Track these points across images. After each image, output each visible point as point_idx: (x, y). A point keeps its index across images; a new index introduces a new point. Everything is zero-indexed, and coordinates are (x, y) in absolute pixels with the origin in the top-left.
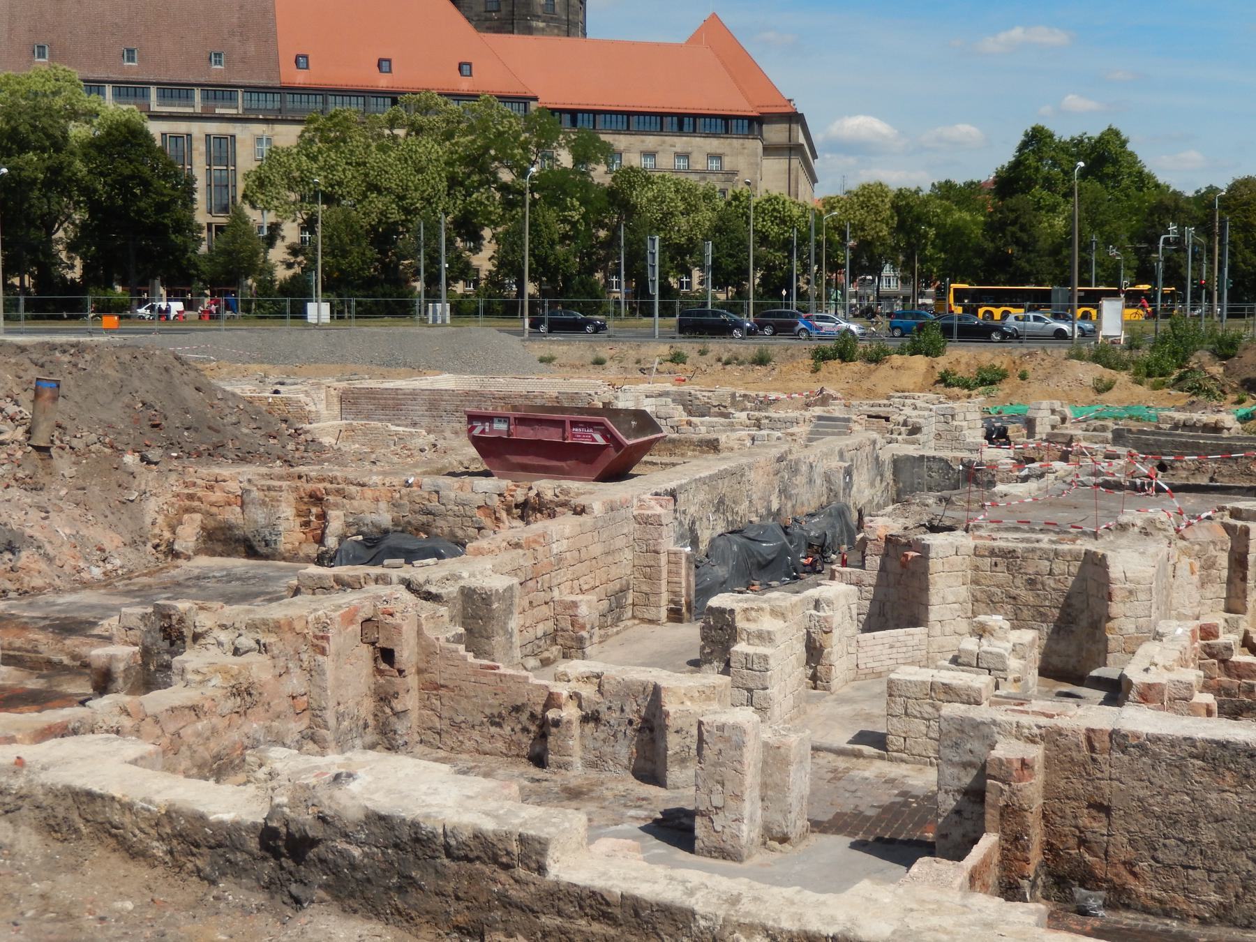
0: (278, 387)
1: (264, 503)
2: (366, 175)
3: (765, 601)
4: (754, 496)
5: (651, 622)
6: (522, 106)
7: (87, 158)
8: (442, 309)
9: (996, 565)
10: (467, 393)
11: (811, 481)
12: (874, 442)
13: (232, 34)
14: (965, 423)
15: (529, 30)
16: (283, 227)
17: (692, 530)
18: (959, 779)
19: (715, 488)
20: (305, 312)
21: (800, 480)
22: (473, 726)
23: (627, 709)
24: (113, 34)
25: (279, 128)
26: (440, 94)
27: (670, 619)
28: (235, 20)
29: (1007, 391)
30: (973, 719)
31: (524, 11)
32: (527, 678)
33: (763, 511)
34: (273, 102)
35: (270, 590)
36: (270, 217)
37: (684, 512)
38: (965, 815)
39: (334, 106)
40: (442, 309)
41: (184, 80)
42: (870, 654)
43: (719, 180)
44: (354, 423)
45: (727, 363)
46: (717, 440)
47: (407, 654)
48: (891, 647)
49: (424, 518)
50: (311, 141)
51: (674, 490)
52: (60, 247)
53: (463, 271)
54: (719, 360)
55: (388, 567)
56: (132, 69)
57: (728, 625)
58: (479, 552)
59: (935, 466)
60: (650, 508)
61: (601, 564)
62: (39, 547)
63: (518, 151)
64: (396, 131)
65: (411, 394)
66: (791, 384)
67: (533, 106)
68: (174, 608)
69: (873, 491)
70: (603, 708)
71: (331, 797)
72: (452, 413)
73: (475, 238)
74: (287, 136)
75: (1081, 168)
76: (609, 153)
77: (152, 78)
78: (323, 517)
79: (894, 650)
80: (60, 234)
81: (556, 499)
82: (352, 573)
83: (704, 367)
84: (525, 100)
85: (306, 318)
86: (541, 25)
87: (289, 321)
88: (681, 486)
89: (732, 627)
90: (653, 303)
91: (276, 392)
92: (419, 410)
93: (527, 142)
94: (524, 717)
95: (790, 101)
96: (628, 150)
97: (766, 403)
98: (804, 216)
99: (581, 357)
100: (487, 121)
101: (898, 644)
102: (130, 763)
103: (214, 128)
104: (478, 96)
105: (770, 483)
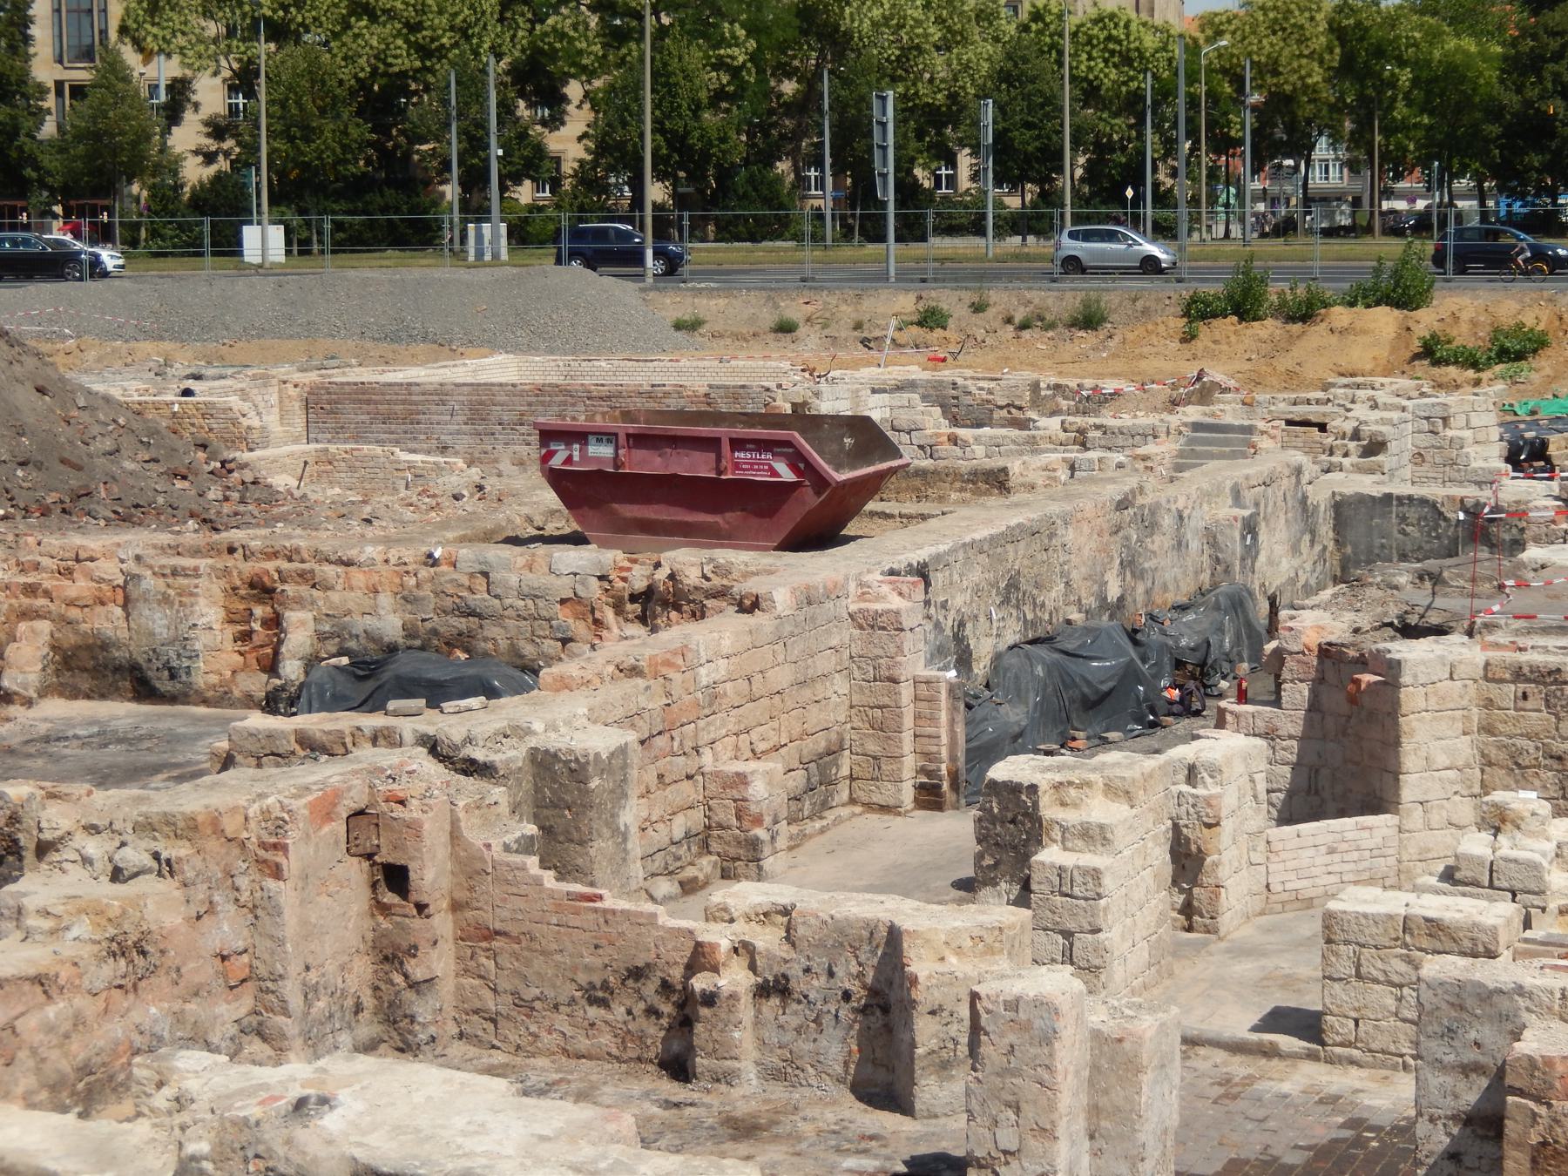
0: (190, 384)
1: (165, 600)
3: (1094, 770)
4: (1075, 575)
5: (885, 809)
9: (1525, 696)
10: (540, 390)
11: (1180, 545)
12: (1298, 471)
14: (1467, 434)
16: (196, 85)
17: (959, 638)
18: (1456, 1097)
19: (1001, 559)
20: (240, 243)
21: (1160, 542)
23: (839, 971)
29: (1548, 371)
30: (1480, 985)
32: (654, 916)
33: (1091, 602)
37: (944, 605)
38: (1468, 1161)
42: (1291, 865)
44: (332, 448)
45: (1024, 326)
46: (1004, 470)
48: (1331, 851)
51: (925, 565)
54: (1009, 321)
55: (396, 714)
57: (1026, 815)
58: (564, 684)
59: (1412, 514)
60: (879, 598)
65: (435, 392)
66: (1143, 364)
69: (1296, 562)
70: (795, 971)
78: (275, 622)
79: (1336, 857)
81: (706, 585)
82: (328, 727)
85: (240, 254)
87: (208, 260)
88: (938, 558)
89: (1033, 817)
90: (884, 217)
91: (187, 392)
94: (650, 988)
98: (1165, 49)
99: (753, 319)
101: (1344, 846)
105: (1104, 549)
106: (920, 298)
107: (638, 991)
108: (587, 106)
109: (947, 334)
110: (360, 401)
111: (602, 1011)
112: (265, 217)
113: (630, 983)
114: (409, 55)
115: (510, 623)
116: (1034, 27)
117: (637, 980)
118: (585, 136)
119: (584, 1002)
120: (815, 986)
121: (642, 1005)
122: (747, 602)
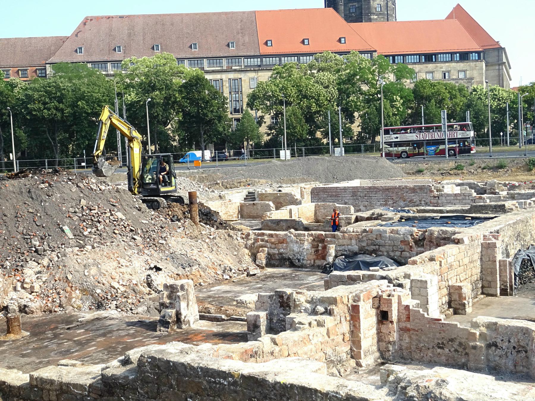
0: (280, 189)
1: (297, 242)
2: (301, 91)
5: (492, 295)
6: (369, 55)
7: (180, 92)
8: (339, 151)
10: (370, 188)
13: (238, 33)
15: (370, 20)
16: (265, 117)
17: (506, 250)
19: (516, 228)
22: (429, 349)
23: (512, 341)
24: (187, 38)
25: (260, 74)
26: (332, 53)
27: (501, 294)
28: (239, 27)
31: (367, 12)
34: (257, 61)
35: (305, 282)
36: (260, 113)
39: (284, 60)
40: (339, 151)
41: (199, 56)
43: (464, 82)
44: (319, 204)
45: (484, 168)
46: (504, 205)
47: (394, 315)
49: (374, 247)
50: (275, 78)
51: (498, 230)
52: (170, 132)
53: (348, 132)
54: (480, 167)
55: (373, 271)
56: (196, 52)
58: (414, 263)
60: (489, 239)
61: (468, 268)
62: (199, 265)
63: (370, 76)
64: (313, 71)
67: (375, 55)
68: (285, 293)
70: (499, 341)
71: (441, 393)
72: (363, 197)
73: (351, 118)
74: (265, 76)
75: (149, 101)
76: (412, 73)
77: (204, 56)
78: (325, 248)
80: (169, 126)
81: (440, 237)
82: (356, 274)
83: (472, 171)
84: (371, 52)
85: (279, 157)
86: (375, 17)
88: (501, 229)
91: (280, 191)
92: (348, 197)
93: (374, 71)
95: (498, 42)
96: (420, 72)
97: (513, 187)
98: (509, 96)
99: (412, 169)
100: (355, 63)
102: (314, 372)
103: (232, 76)
104: (349, 52)
106: (456, 162)
107: (452, 345)
108: (359, 118)
109: (463, 171)
110: (324, 192)
111: (442, 350)
112: (286, 148)
113: (450, 343)
114: (173, 118)
115: (387, 247)
116: (474, 93)
117: (452, 342)
118: (359, 126)
119: (436, 348)
120: (505, 345)
121: (453, 349)
122: (456, 241)
